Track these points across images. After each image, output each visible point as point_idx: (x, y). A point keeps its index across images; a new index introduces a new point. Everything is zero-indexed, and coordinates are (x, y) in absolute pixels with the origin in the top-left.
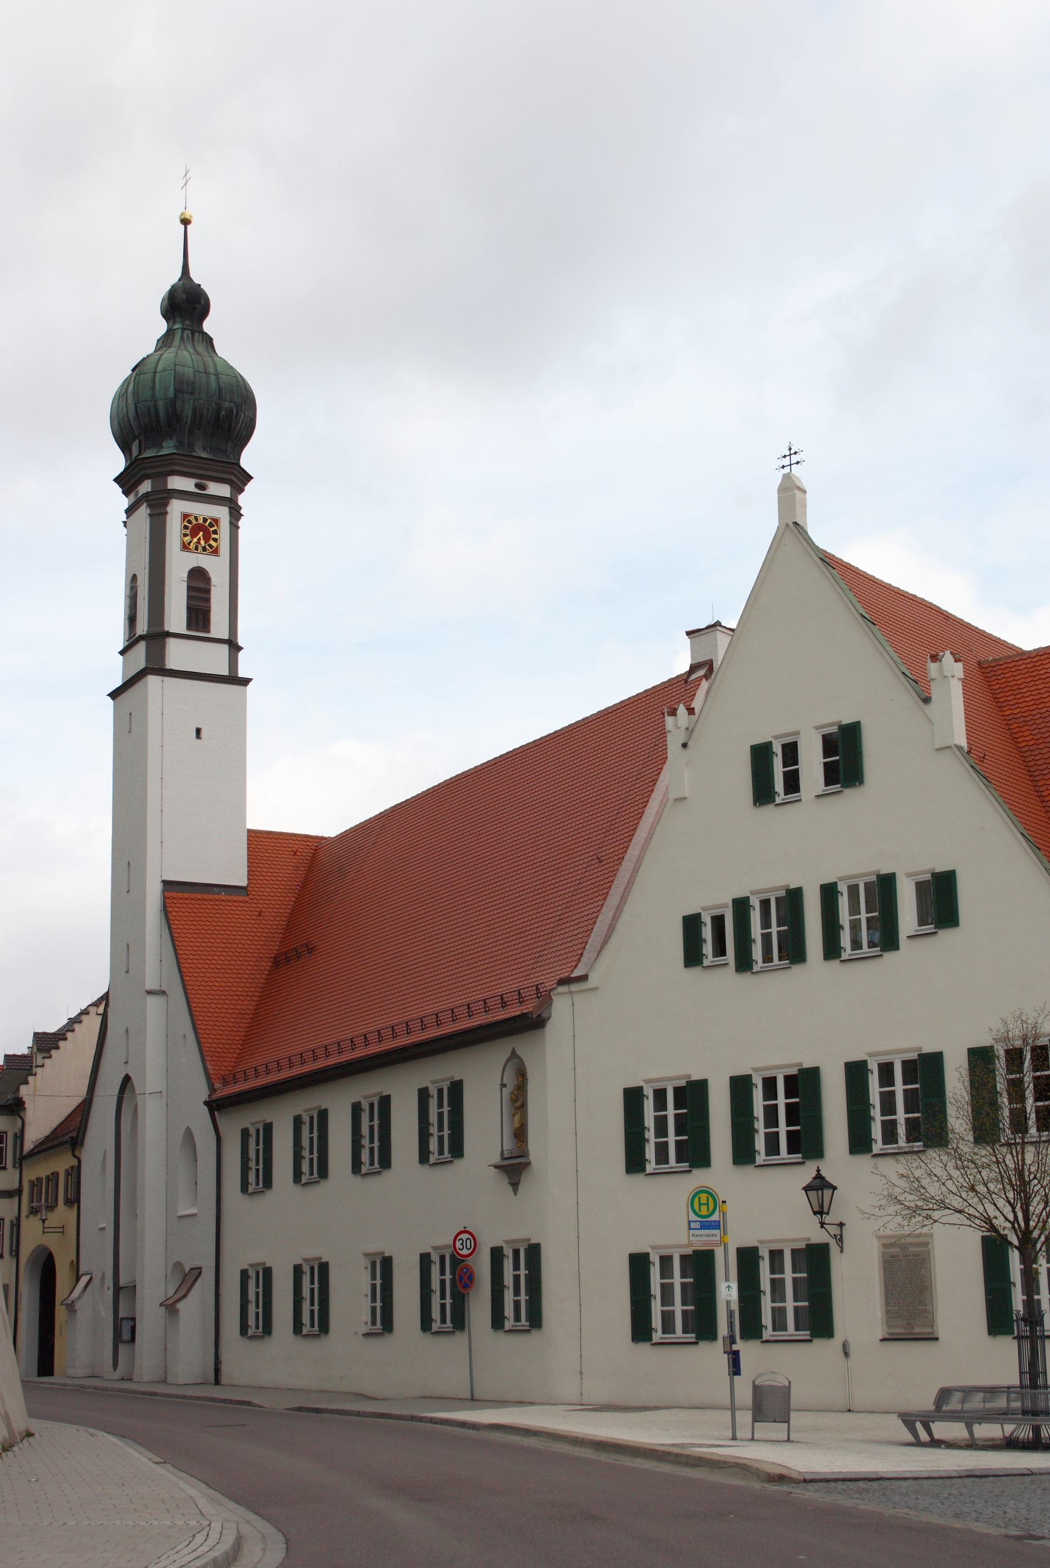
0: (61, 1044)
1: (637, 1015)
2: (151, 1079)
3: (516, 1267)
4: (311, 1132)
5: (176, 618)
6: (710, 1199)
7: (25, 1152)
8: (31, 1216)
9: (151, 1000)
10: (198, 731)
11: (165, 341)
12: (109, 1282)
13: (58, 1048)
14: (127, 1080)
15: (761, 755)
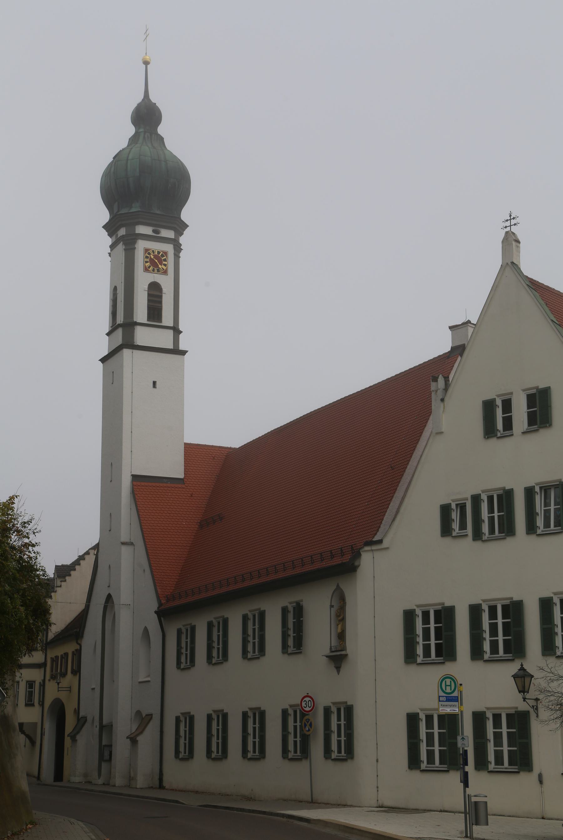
0: (72, 573)
1: (411, 565)
2: (124, 596)
3: (339, 719)
4: (219, 631)
5: (141, 313)
6: (452, 682)
7: (49, 640)
8: (52, 680)
9: (124, 548)
10: (154, 383)
11: (133, 140)
12: (97, 723)
13: (70, 575)
14: (109, 597)
15: (488, 407)
